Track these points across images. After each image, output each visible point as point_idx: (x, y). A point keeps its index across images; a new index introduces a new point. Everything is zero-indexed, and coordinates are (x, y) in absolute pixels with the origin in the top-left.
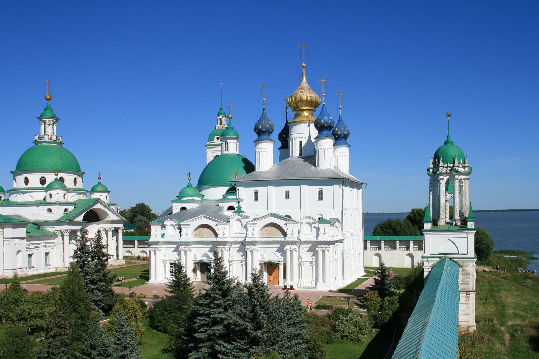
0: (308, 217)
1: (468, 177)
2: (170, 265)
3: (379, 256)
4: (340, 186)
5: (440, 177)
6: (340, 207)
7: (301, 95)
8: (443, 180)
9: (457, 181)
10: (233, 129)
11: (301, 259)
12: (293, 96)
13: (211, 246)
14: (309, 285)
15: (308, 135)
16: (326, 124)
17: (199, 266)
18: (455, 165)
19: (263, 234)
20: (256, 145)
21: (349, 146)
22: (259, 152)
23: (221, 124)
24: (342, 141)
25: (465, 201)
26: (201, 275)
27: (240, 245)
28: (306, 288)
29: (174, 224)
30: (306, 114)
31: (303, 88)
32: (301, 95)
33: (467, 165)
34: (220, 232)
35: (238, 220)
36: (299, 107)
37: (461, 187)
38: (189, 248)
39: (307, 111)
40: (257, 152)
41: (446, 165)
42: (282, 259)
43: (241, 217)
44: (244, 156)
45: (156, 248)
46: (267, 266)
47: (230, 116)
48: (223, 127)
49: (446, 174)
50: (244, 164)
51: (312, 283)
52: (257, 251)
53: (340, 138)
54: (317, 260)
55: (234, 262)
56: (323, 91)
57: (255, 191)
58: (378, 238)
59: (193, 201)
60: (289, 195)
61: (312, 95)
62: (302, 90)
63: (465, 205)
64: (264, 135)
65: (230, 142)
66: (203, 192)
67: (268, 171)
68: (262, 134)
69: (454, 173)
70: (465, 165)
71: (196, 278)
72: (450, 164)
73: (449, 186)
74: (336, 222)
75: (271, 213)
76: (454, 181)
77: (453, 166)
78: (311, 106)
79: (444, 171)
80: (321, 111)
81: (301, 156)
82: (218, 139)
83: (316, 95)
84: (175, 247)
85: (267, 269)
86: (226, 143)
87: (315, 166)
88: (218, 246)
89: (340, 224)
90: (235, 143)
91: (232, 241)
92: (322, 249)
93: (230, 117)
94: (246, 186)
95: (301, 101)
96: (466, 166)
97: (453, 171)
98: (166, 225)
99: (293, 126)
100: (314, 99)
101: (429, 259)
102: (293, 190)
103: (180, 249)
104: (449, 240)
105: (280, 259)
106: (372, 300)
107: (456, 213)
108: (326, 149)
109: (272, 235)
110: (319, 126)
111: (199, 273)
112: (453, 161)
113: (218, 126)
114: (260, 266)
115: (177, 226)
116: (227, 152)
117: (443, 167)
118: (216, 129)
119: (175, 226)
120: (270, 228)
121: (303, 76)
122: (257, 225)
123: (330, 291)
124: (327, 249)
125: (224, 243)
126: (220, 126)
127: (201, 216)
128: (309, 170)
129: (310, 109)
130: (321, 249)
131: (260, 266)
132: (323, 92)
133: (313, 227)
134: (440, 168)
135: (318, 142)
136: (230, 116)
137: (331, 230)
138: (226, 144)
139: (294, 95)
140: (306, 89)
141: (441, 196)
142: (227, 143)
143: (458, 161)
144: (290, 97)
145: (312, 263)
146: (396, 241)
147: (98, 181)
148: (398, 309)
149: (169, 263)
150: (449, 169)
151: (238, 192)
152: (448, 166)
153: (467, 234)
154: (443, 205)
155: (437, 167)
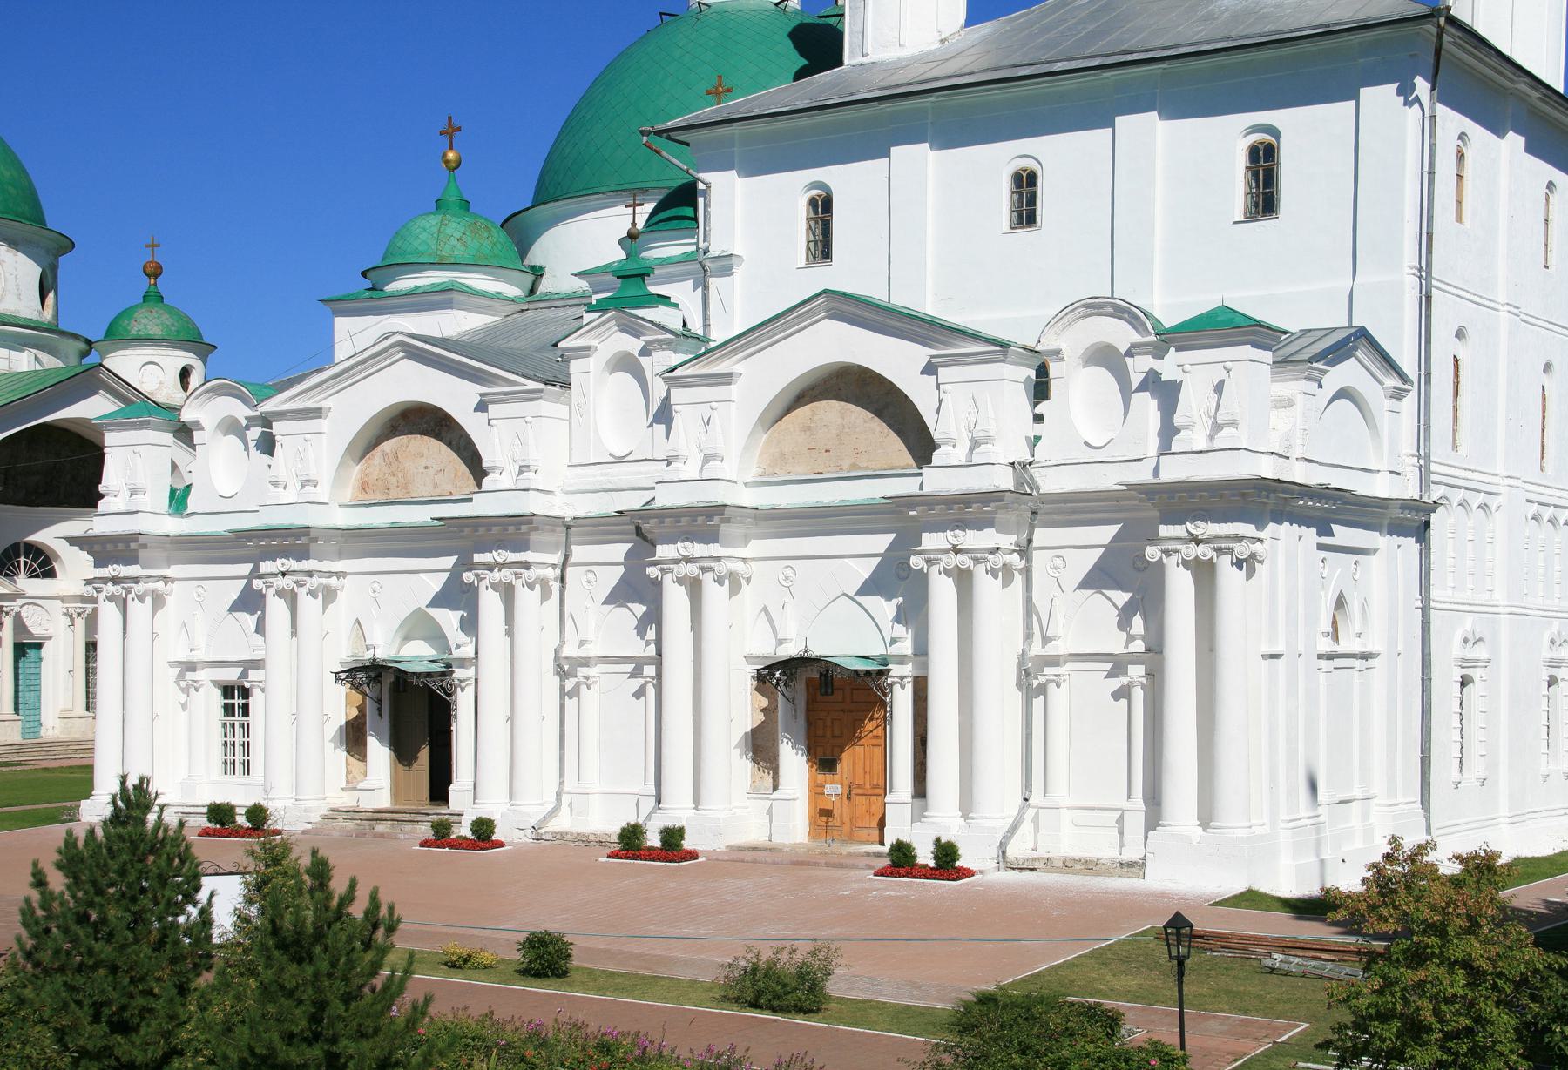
0: (1094, 308)
2: (217, 699)
4: (1406, 91)
6: (1409, 254)
11: (1046, 640)
14: (1104, 848)
19: (783, 454)
27: (629, 545)
28: (1068, 866)
29: (241, 412)
35: (626, 364)
38: (310, 574)
42: (906, 647)
45: (126, 578)
46: (802, 704)
50: (802, 54)
51: (1121, 833)
52: (734, 583)
54: (1155, 649)
55: (591, 672)
57: (815, 192)
75: (825, 292)
84: (630, 670)
85: (810, 723)
88: (478, 558)
89: (1392, 382)
91: (568, 514)
92: (1192, 551)
94: (758, 164)
98: (197, 424)
105: (894, 641)
109: (846, 464)
111: (379, 752)
114: (765, 702)
120: (831, 412)
122: (734, 390)
123: (1251, 899)
124: (1230, 551)
130: (1183, 548)
131: (765, 702)
133: (1136, 380)
137: (1289, 403)
145: (1125, 674)
147: (145, 283)
149: (216, 683)
151: (706, 206)
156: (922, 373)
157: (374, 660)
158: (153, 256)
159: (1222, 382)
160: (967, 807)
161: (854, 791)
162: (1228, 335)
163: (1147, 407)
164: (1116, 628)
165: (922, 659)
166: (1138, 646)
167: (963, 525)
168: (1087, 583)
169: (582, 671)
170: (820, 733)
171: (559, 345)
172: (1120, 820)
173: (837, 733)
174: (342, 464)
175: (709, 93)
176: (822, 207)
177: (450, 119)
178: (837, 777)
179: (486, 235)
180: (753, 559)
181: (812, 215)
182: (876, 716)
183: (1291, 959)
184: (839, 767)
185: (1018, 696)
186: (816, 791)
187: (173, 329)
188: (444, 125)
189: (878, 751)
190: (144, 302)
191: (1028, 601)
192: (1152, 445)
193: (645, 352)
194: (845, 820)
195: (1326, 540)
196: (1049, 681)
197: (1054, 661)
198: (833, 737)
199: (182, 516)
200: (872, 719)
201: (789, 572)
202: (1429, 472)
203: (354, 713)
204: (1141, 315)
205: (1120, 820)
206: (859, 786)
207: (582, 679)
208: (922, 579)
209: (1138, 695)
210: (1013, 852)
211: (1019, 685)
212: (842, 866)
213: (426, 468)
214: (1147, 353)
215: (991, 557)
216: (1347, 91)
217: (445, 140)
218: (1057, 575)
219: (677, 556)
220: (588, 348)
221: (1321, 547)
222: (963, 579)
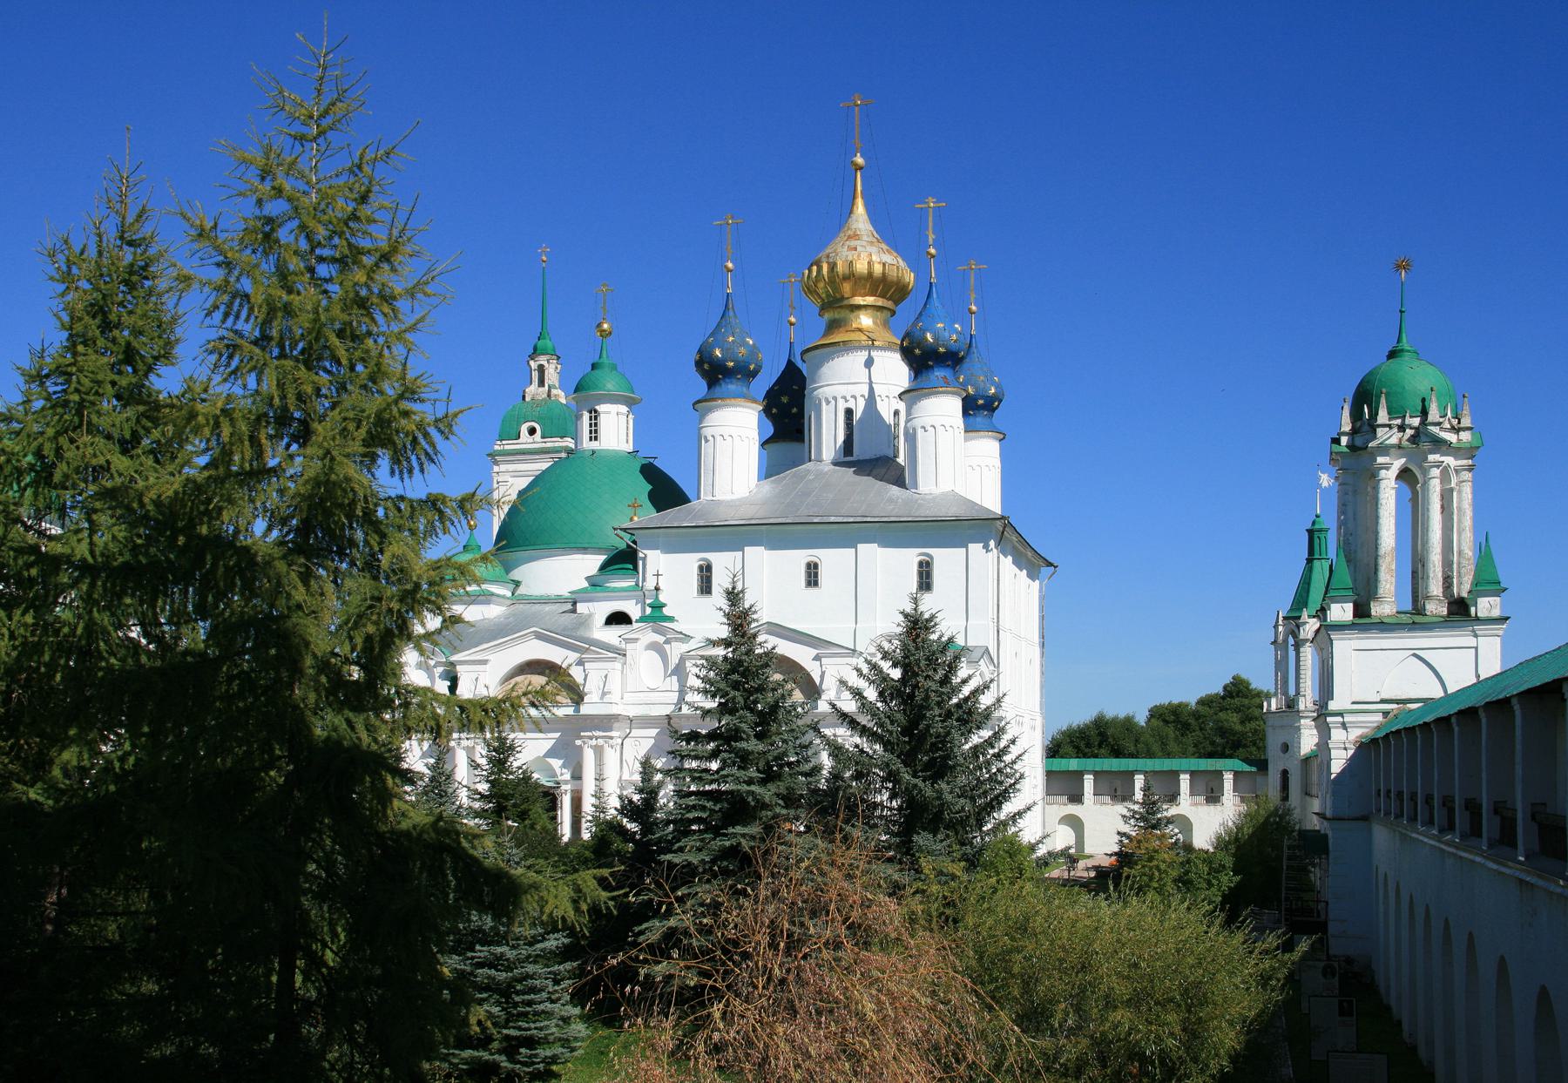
1: (1470, 462)
3: (1075, 823)
4: (986, 547)
5: (1380, 460)
6: (992, 612)
7: (850, 258)
8: (1387, 469)
9: (1435, 472)
10: (616, 369)
12: (824, 260)
13: (557, 735)
15: (865, 390)
16: (943, 346)
18: (1430, 419)
20: (701, 419)
21: (1002, 436)
22: (713, 436)
23: (541, 383)
24: (979, 419)
25: (1459, 541)
30: (865, 320)
31: (856, 236)
32: (851, 256)
33: (1466, 422)
34: (592, 690)
35: (654, 646)
36: (843, 298)
37: (1446, 496)
39: (869, 311)
40: (706, 437)
41: (1399, 421)
43: (664, 639)
44: (651, 460)
47: (606, 326)
48: (549, 395)
49: (1401, 451)
53: (973, 410)
56: (931, 237)
57: (701, 563)
58: (1073, 764)
59: (486, 598)
60: (816, 575)
61: (889, 258)
62: (853, 243)
63: (1460, 553)
64: (731, 383)
65: (605, 413)
66: (516, 574)
67: (742, 502)
68: (724, 377)
69: (1426, 446)
70: (1459, 423)
72: (1411, 417)
73: (1311, 593)
74: (982, 657)
76: (1425, 472)
77: (1424, 422)
78: (883, 296)
79: (1394, 440)
80: (925, 304)
81: (849, 459)
82: (532, 431)
83: (900, 260)
86: (593, 414)
87: (900, 481)
90: (623, 414)
93: (604, 331)
94: (671, 548)
95: (851, 276)
96: (1462, 425)
97: (1423, 440)
99: (819, 365)
100: (893, 274)
101: (1348, 718)
102: (832, 560)
104: (1414, 655)
106: (1151, 859)
107: (1431, 575)
108: (940, 430)
110: (917, 351)
112: (1420, 408)
113: (532, 389)
115: (440, 669)
116: (594, 445)
117: (1390, 426)
118: (527, 399)
121: (854, 198)
125: (605, 722)
126: (541, 389)
127: (529, 631)
128: (884, 499)
129: (880, 304)
132: (931, 241)
134: (1380, 431)
135: (914, 407)
136: (606, 326)
138: (591, 419)
139: (828, 257)
140: (865, 238)
141: (1381, 521)
142: (595, 416)
143: (1439, 407)
144: (812, 265)
146: (1132, 774)
148: (1236, 887)
150: (1409, 432)
152: (1407, 422)
153: (1476, 636)
154: (1390, 548)
155: (1366, 428)
157: (1133, 717)
193: (667, 642)
216: (963, 544)
220: (637, 639)
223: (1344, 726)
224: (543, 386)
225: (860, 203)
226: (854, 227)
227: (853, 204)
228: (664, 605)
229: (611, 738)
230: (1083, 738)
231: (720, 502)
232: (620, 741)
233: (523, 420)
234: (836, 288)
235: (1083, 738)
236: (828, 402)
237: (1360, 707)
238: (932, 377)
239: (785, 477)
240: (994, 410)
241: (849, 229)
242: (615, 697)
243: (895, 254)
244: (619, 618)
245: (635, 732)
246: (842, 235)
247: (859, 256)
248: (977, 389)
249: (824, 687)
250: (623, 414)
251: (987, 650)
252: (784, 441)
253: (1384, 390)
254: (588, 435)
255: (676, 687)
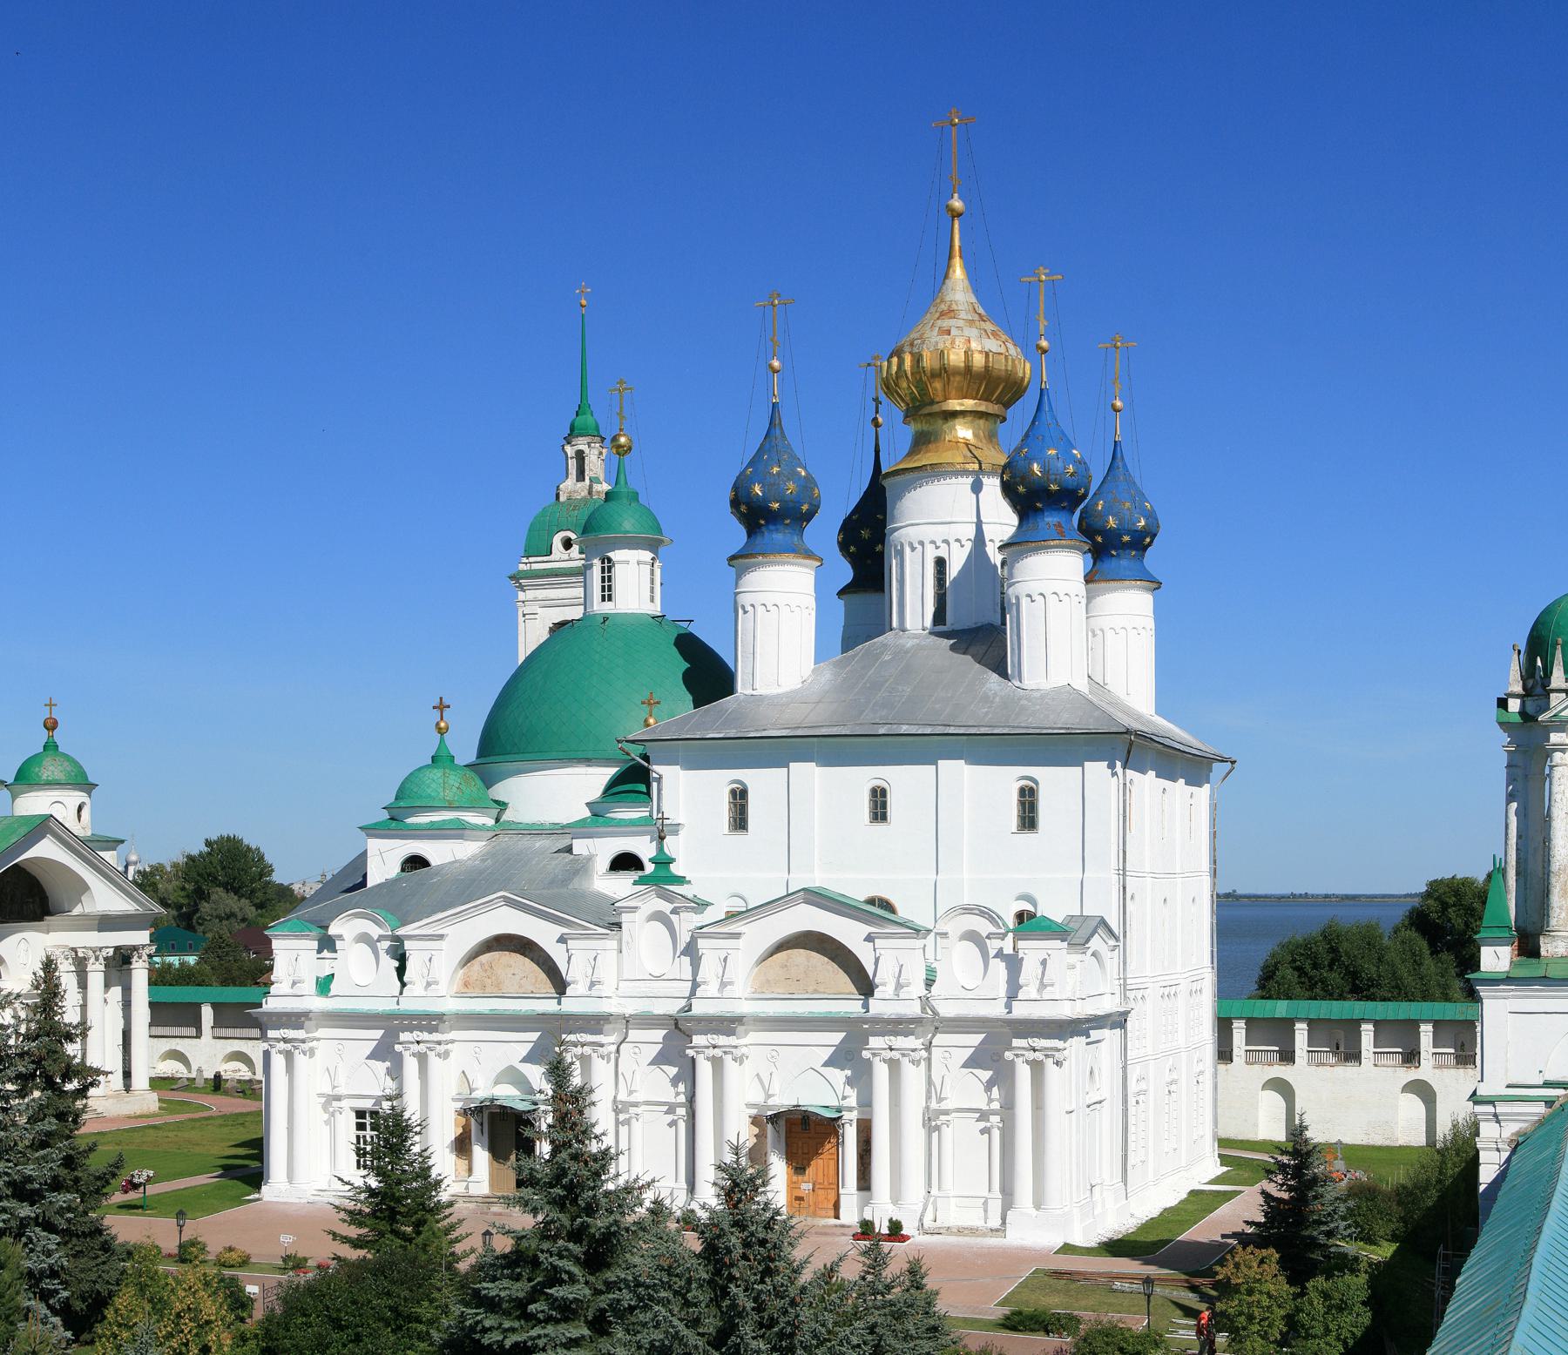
4: (1112, 766)
7: (941, 346)
11: (940, 1100)
12: (907, 349)
13: (535, 1036)
14: (974, 1219)
16: (1055, 481)
17: (482, 1124)
19: (768, 981)
20: (739, 577)
21: (1155, 585)
23: (581, 475)
26: (491, 1165)
28: (960, 1231)
30: (964, 431)
31: (950, 313)
32: (942, 342)
35: (658, 916)
38: (439, 1043)
39: (969, 419)
40: (743, 607)
42: (852, 1101)
43: (671, 906)
47: (623, 440)
48: (590, 492)
51: (986, 1211)
52: (740, 1060)
53: (1116, 550)
54: (1008, 1106)
58: (1281, 1008)
59: (457, 831)
61: (993, 345)
62: (946, 323)
64: (777, 530)
66: (501, 790)
67: (791, 698)
68: (767, 522)
71: (471, 1179)
75: (803, 889)
78: (986, 398)
81: (941, 628)
82: (567, 544)
83: (1010, 346)
89: (1112, 942)
90: (645, 563)
92: (1031, 1055)
95: (943, 372)
98: (340, 937)
100: (1000, 365)
101: (1501, 1108)
102: (904, 781)
103: (398, 1048)
105: (844, 1098)
106: (1250, 1292)
109: (810, 989)
111: (481, 1155)
113: (570, 485)
114: (756, 1131)
115: (386, 944)
116: (607, 608)
118: (562, 498)
119: (378, 941)
120: (800, 956)
121: (950, 257)
122: (740, 943)
123: (1067, 1249)
124: (1053, 1056)
125: (594, 1023)
126: (580, 484)
131: (756, 1131)
133: (992, 953)
136: (623, 440)
137: (1073, 967)
139: (912, 345)
140: (963, 315)
142: (608, 566)
144: (891, 356)
155: (1538, 690)
156: (864, 940)
158: (51, 713)
159: (1045, 959)
160: (896, 1198)
161: (817, 1186)
162: (1048, 935)
163: (999, 969)
164: (1192, 1189)
165: (866, 1109)
166: (996, 1105)
167: (896, 1034)
168: (965, 1065)
169: (633, 1110)
170: (794, 1151)
171: (616, 905)
172: (985, 1203)
173: (806, 1151)
174: (455, 971)
175: (643, 703)
176: (739, 797)
177: (441, 699)
178: (806, 1178)
179: (473, 783)
180: (751, 1045)
181: (731, 801)
182: (832, 1140)
183: (1124, 1284)
184: (807, 1172)
185: (922, 1133)
186: (792, 1186)
187: (73, 774)
188: (437, 702)
189: (832, 1163)
190: (44, 750)
191: (929, 1078)
192: (1002, 991)
194: (811, 1203)
195: (1089, 1040)
196: (942, 1124)
197: (946, 1112)
198: (803, 1153)
199: (327, 996)
200: (829, 1142)
201: (774, 1053)
202: (1125, 984)
203: (460, 1131)
204: (996, 917)
205: (985, 1203)
206: (820, 1184)
207: (633, 1115)
208: (868, 1065)
209: (996, 1134)
210: (928, 1223)
211: (924, 1126)
212: (826, 1234)
213: (514, 974)
214: (998, 938)
215: (912, 1053)
217: (437, 713)
218: (946, 1062)
219: (707, 1044)
221: (1088, 1044)
222: (894, 1065)
223: (1496, 1118)
224: (584, 480)
225: (957, 262)
226: (948, 298)
227: (949, 266)
228: (672, 860)
229: (602, 1046)
230: (1308, 957)
231: (759, 699)
232: (613, 1048)
233: (556, 529)
234: (923, 390)
235: (1308, 957)
236: (913, 549)
237: (1517, 1094)
238: (1041, 525)
239: (855, 656)
240: (1145, 548)
241: (942, 301)
242: (605, 990)
243: (1004, 337)
244: (625, 862)
245: (634, 1034)
246: (933, 310)
247: (953, 342)
248: (1121, 521)
249: (877, 981)
250: (645, 563)
251: (1103, 922)
252: (865, 591)
253: (1560, 641)
254: (600, 594)
255: (687, 973)
